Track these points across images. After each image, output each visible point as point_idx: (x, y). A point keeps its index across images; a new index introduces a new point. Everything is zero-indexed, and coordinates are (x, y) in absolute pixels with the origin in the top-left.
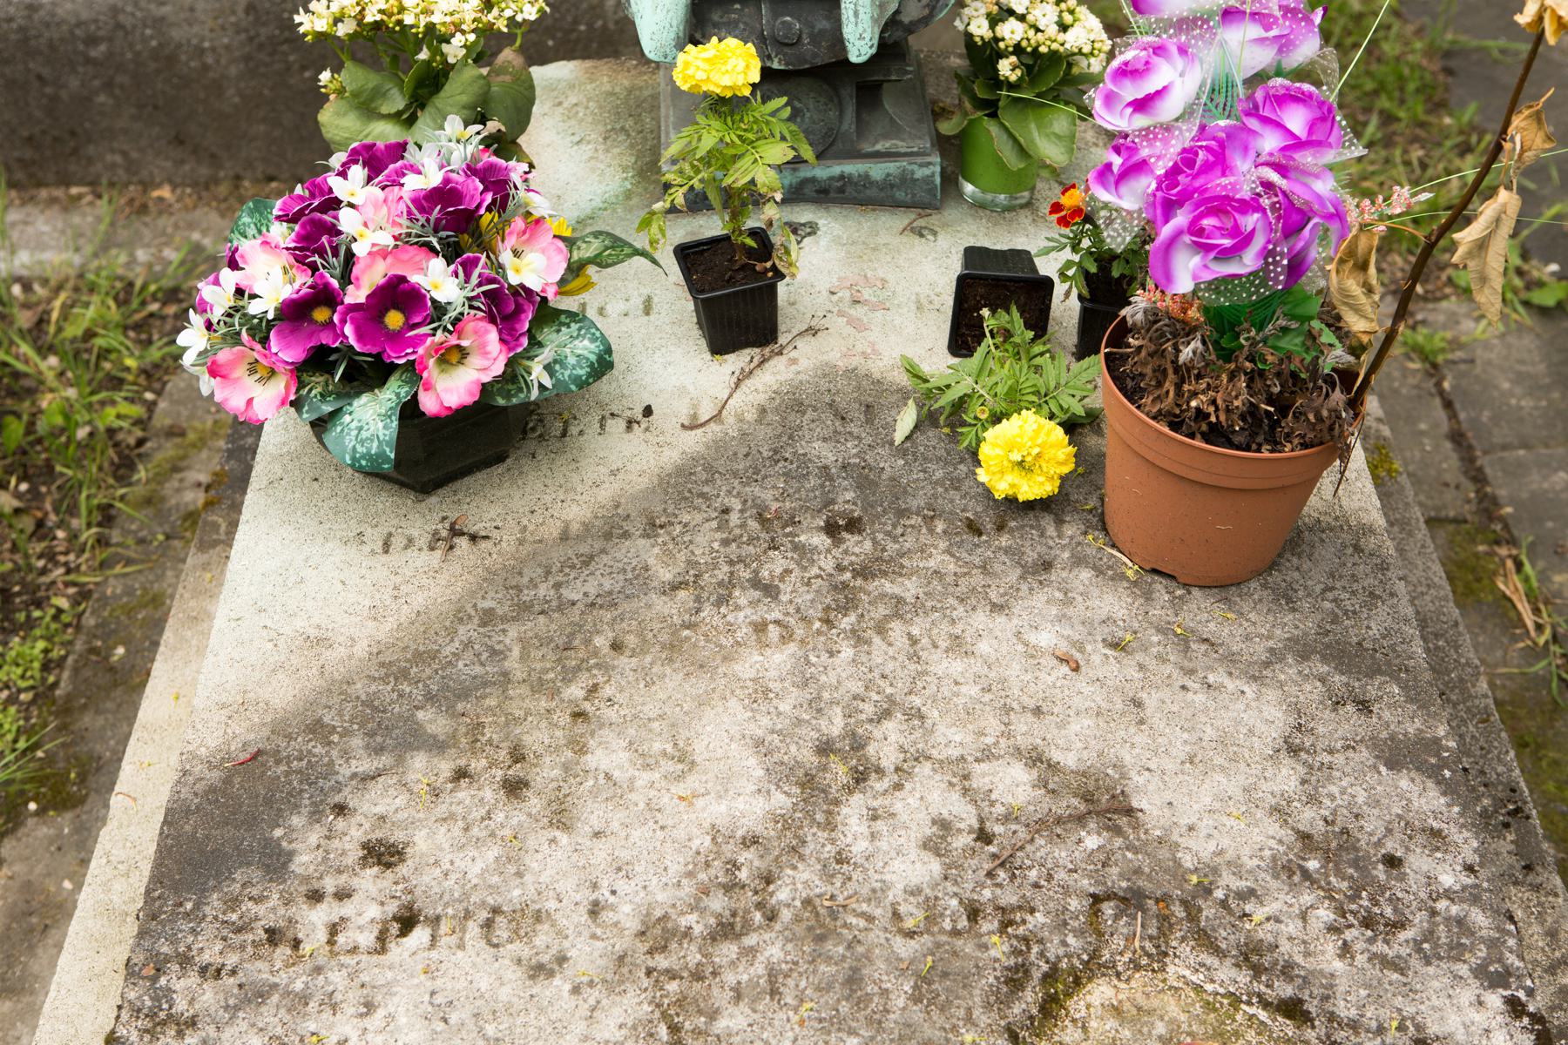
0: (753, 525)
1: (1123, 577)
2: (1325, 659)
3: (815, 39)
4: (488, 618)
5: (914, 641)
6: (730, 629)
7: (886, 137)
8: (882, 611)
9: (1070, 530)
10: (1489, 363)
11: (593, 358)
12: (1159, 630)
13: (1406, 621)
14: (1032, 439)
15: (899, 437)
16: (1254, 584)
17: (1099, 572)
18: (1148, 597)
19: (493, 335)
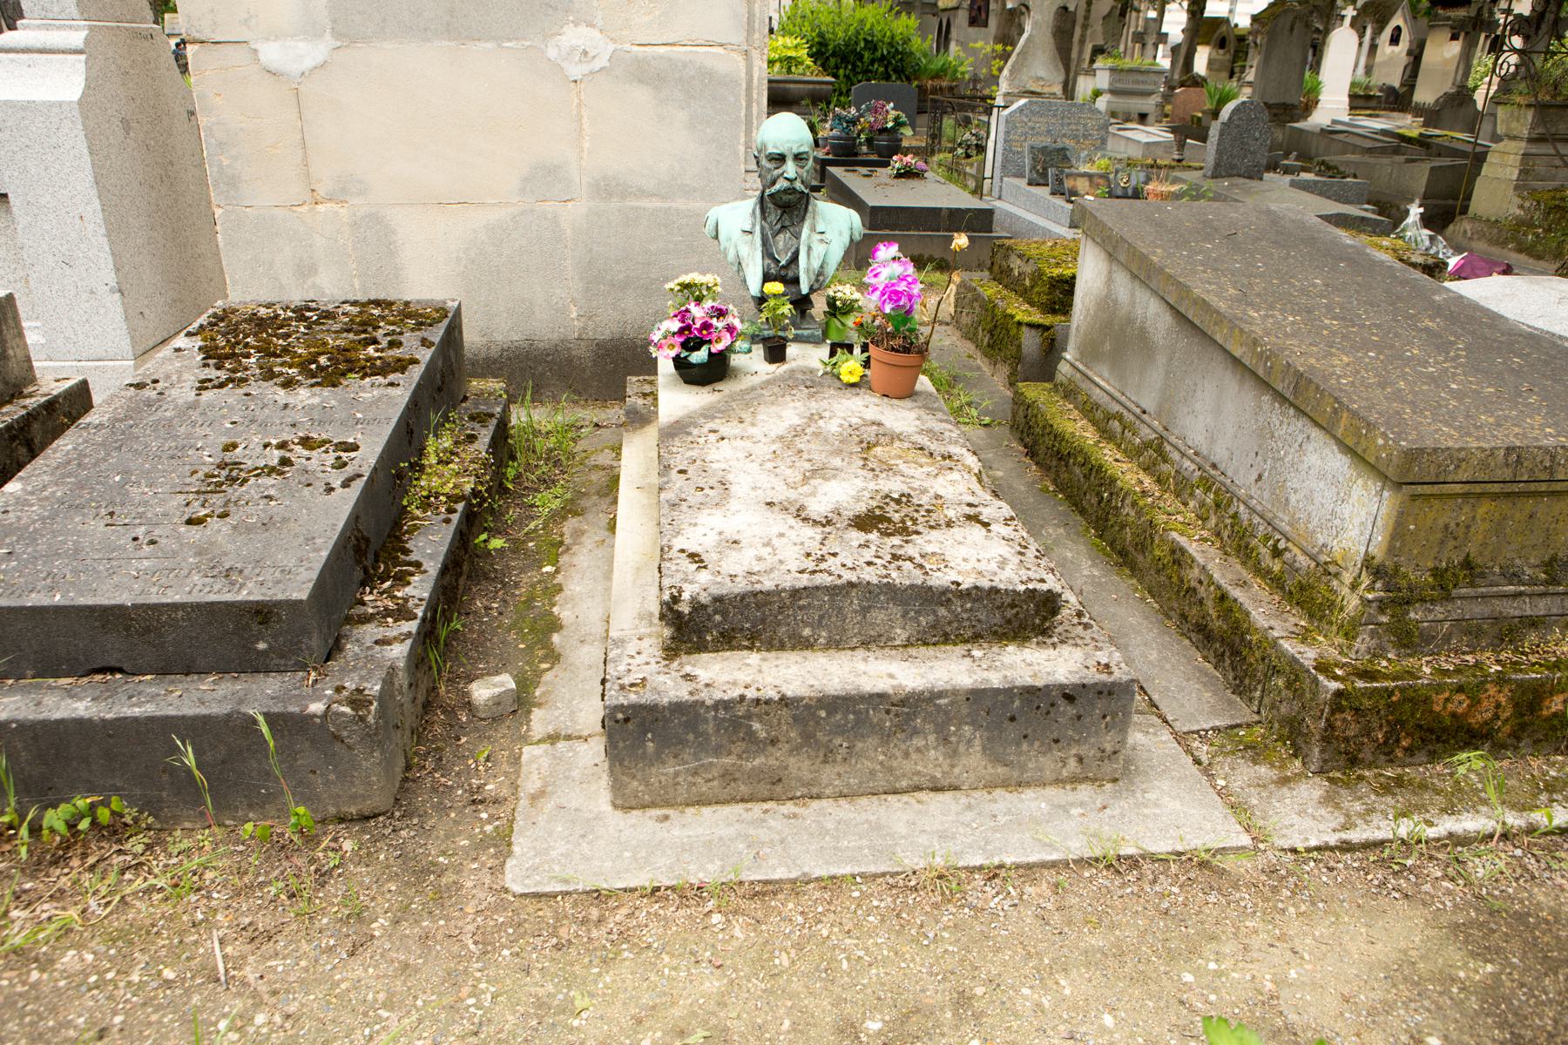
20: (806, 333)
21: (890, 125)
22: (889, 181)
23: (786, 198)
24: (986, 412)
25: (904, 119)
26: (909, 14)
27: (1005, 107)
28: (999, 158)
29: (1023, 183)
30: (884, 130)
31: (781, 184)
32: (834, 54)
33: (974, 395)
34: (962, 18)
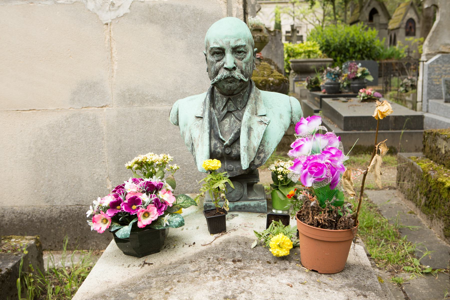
0: (215, 261)
1: (305, 272)
2: (355, 287)
3: (236, 170)
4: (149, 277)
5: (251, 280)
6: (206, 278)
7: (254, 196)
8: (244, 275)
9: (292, 264)
10: (414, 284)
11: (180, 221)
12: (313, 281)
13: (376, 282)
14: (282, 239)
15: (252, 247)
16: (337, 274)
17: (299, 271)
18: (311, 275)
19: (156, 209)
20: (252, 203)
21: (359, 75)
22: (359, 104)
23: (227, 86)
24: (427, 261)
25: (367, 71)
26: (372, 29)
27: (426, 61)
28: (425, 89)
29: (442, 102)
30: (356, 78)
31: (223, 73)
32: (334, 50)
33: (416, 246)
34: (402, 32)
